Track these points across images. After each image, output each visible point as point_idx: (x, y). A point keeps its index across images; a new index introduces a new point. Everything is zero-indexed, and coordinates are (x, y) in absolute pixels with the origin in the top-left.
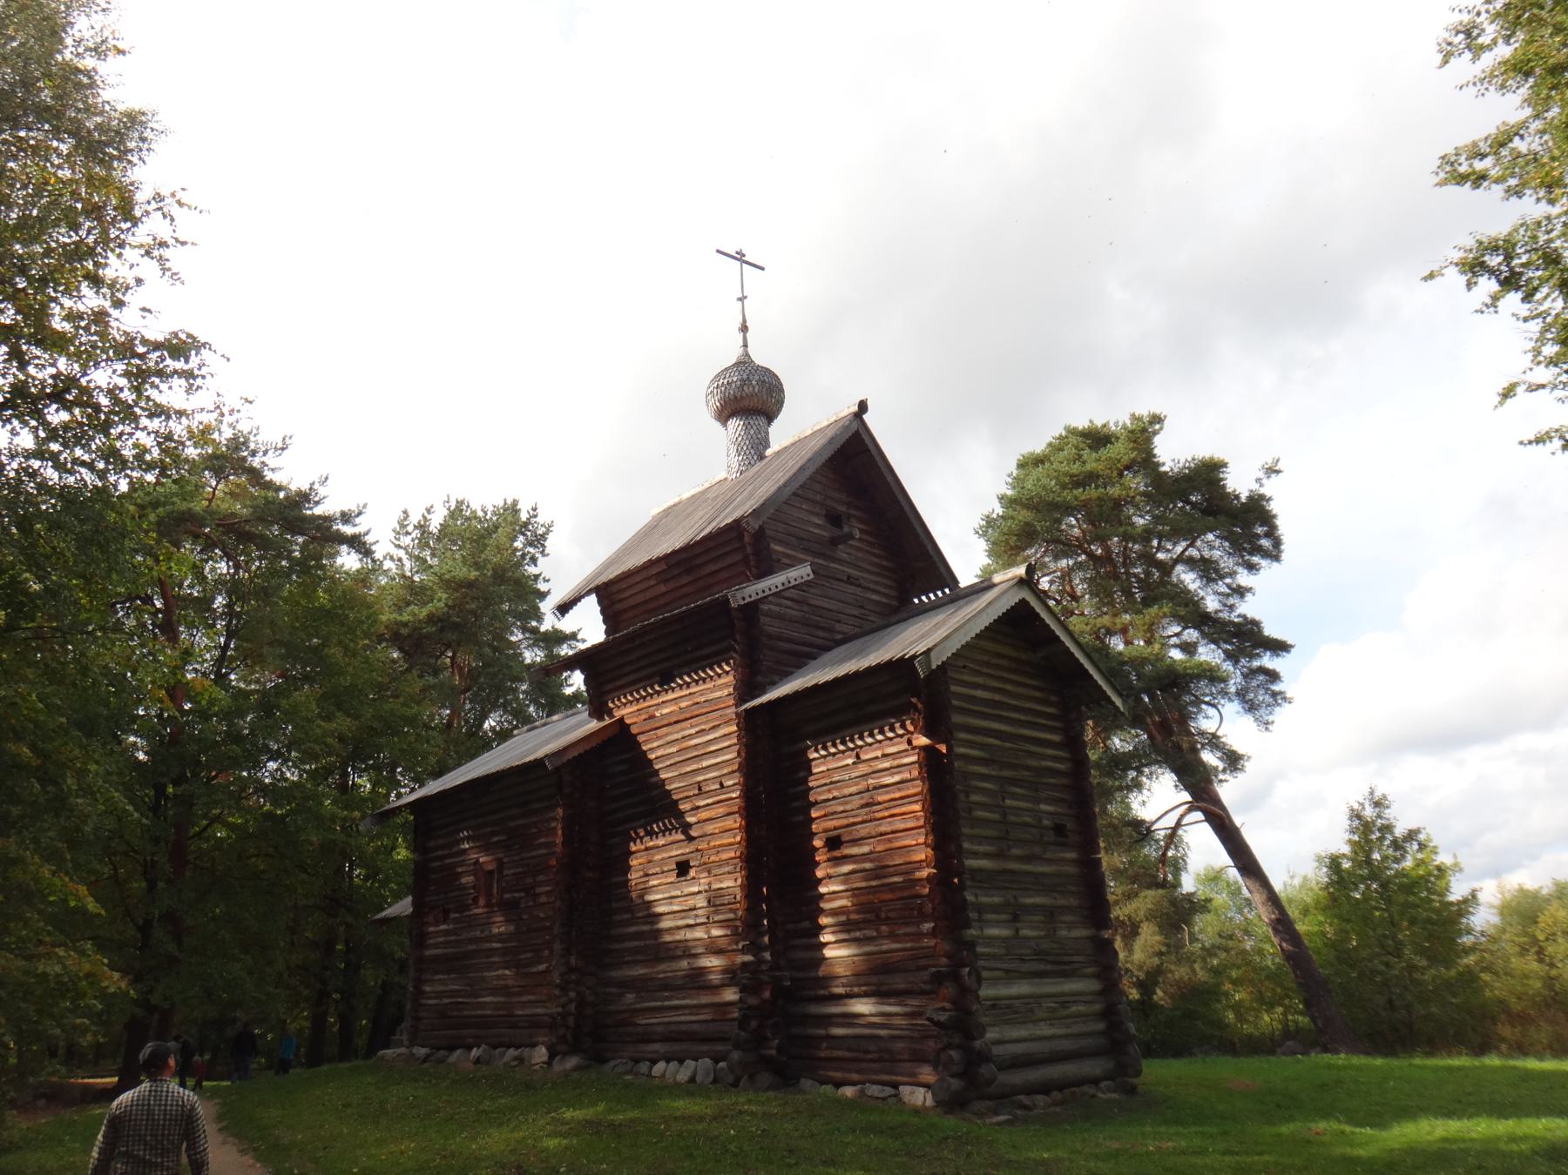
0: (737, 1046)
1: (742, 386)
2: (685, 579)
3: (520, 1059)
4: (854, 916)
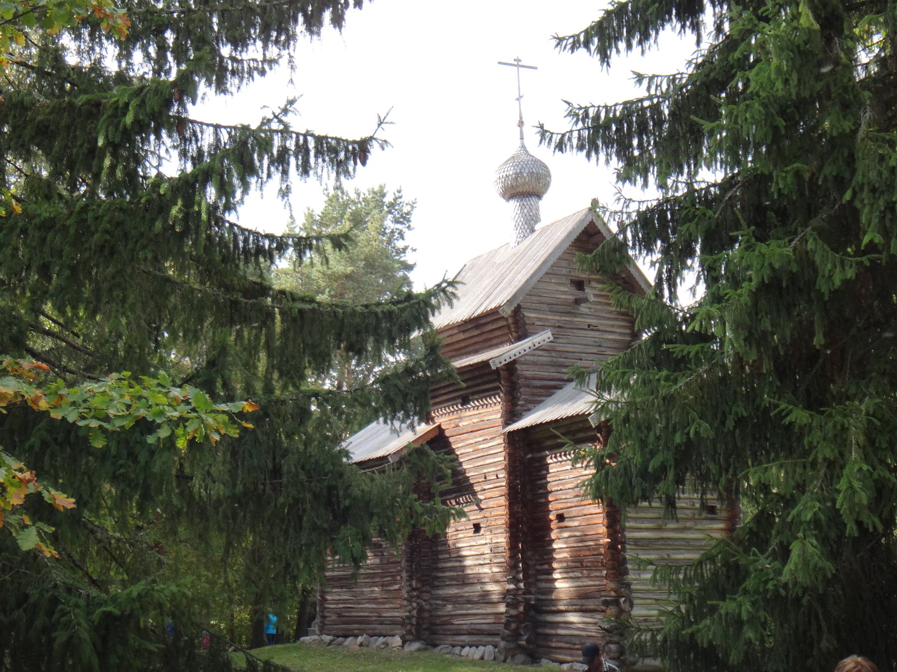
0: (503, 639)
1: (516, 178)
2: (476, 332)
3: (386, 644)
4: (570, 564)
